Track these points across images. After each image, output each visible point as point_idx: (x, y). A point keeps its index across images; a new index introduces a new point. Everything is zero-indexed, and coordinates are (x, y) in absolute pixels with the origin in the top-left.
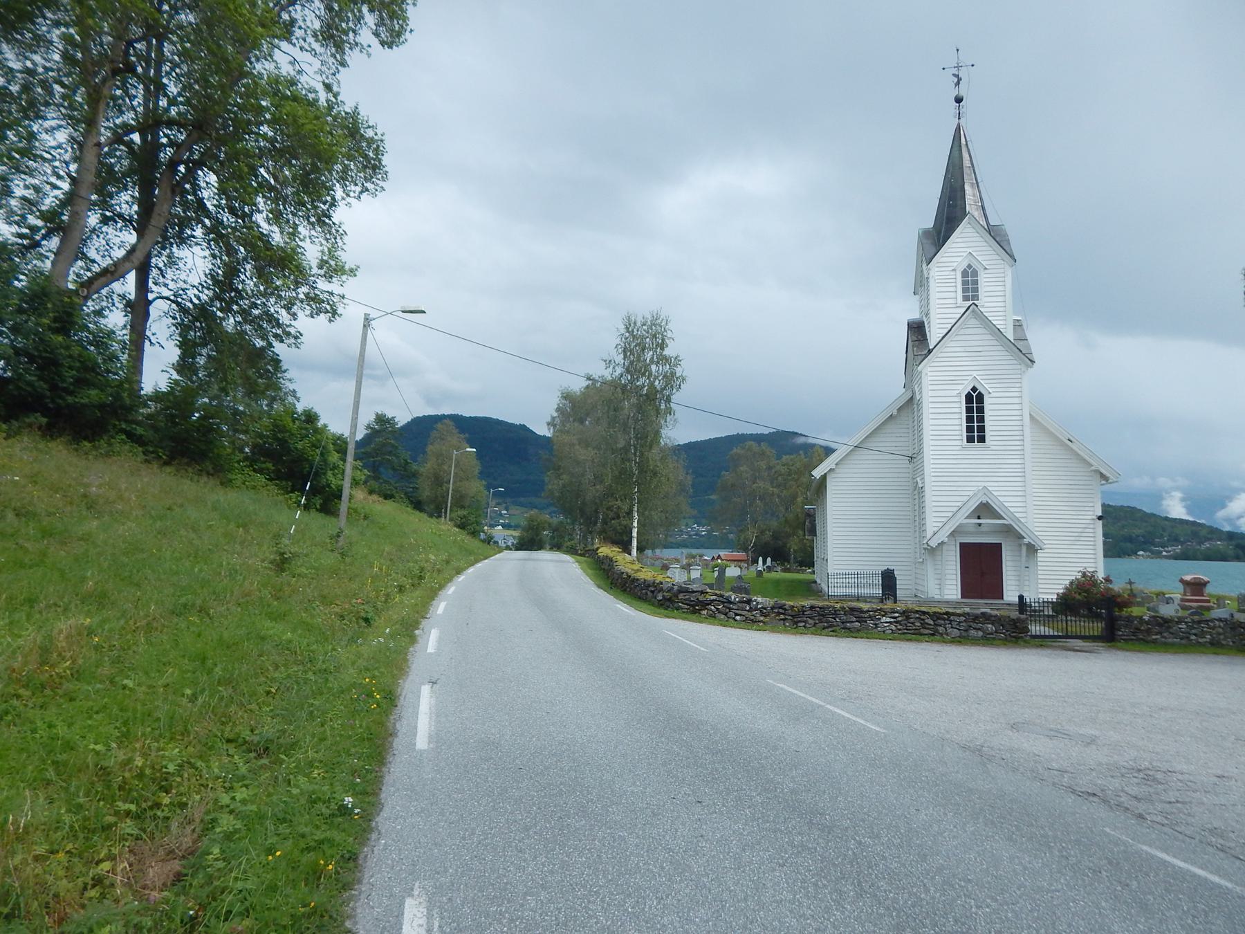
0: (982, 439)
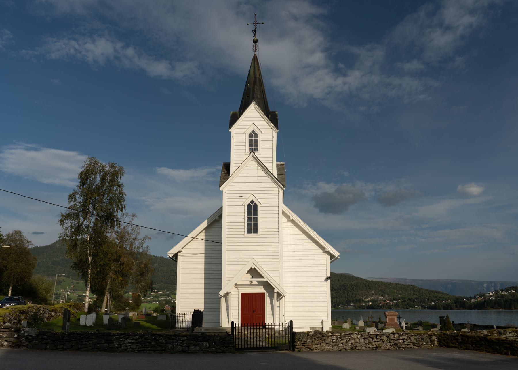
0: (256, 231)
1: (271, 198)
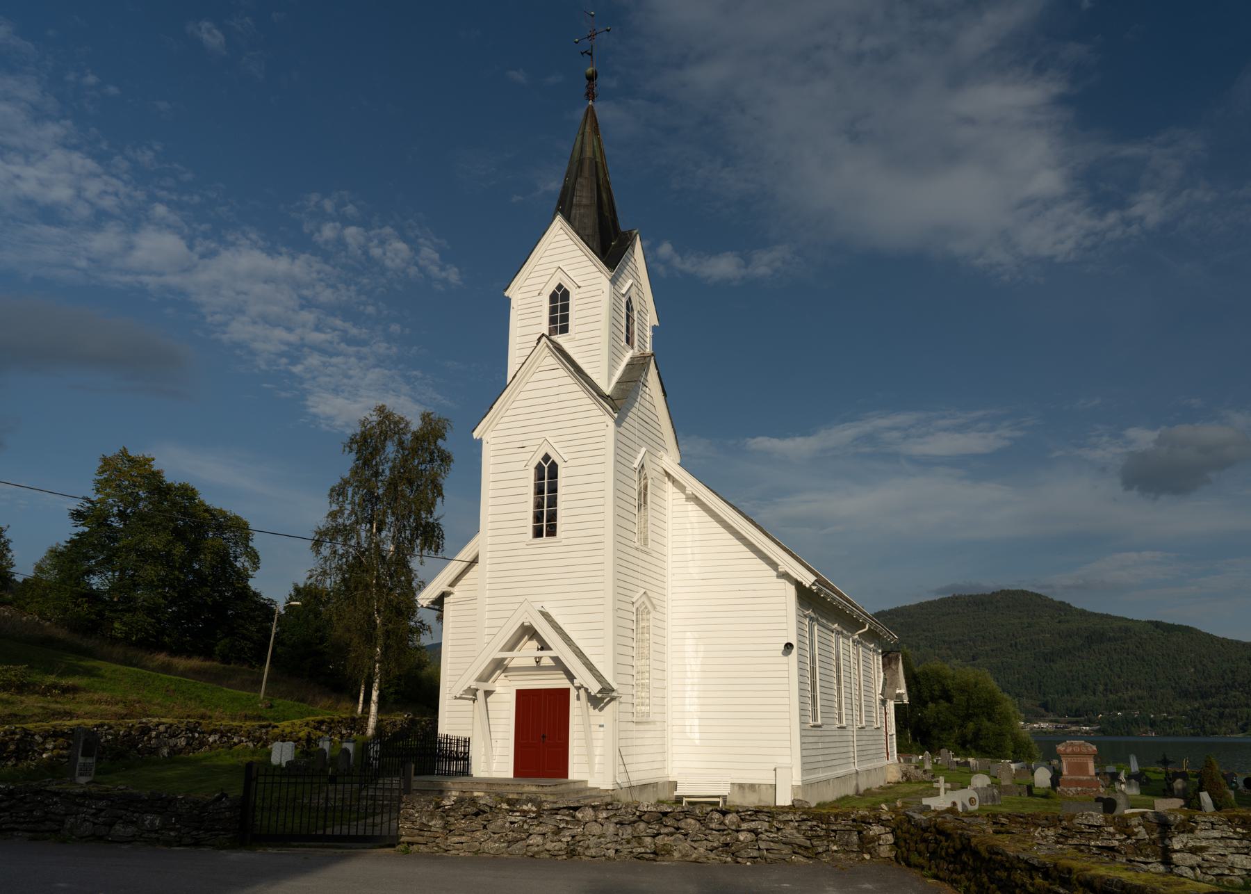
0: (552, 532)
1: (588, 446)
